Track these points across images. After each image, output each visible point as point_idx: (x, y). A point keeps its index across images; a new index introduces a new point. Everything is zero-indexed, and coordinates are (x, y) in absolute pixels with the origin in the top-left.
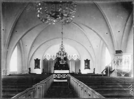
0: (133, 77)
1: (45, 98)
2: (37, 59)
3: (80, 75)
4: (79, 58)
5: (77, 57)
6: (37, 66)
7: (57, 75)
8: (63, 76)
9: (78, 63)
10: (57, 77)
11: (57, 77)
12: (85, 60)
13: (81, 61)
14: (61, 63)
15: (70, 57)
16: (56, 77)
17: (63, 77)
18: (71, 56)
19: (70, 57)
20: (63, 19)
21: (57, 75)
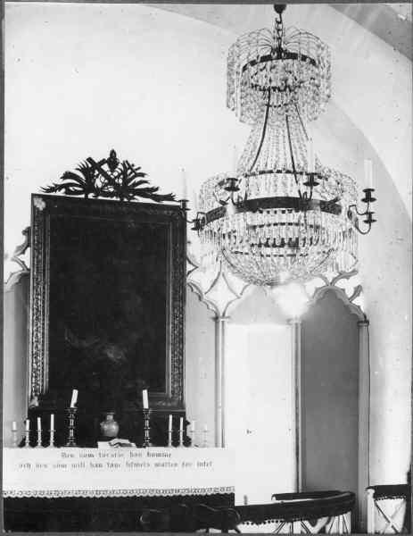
4: (347, 286)
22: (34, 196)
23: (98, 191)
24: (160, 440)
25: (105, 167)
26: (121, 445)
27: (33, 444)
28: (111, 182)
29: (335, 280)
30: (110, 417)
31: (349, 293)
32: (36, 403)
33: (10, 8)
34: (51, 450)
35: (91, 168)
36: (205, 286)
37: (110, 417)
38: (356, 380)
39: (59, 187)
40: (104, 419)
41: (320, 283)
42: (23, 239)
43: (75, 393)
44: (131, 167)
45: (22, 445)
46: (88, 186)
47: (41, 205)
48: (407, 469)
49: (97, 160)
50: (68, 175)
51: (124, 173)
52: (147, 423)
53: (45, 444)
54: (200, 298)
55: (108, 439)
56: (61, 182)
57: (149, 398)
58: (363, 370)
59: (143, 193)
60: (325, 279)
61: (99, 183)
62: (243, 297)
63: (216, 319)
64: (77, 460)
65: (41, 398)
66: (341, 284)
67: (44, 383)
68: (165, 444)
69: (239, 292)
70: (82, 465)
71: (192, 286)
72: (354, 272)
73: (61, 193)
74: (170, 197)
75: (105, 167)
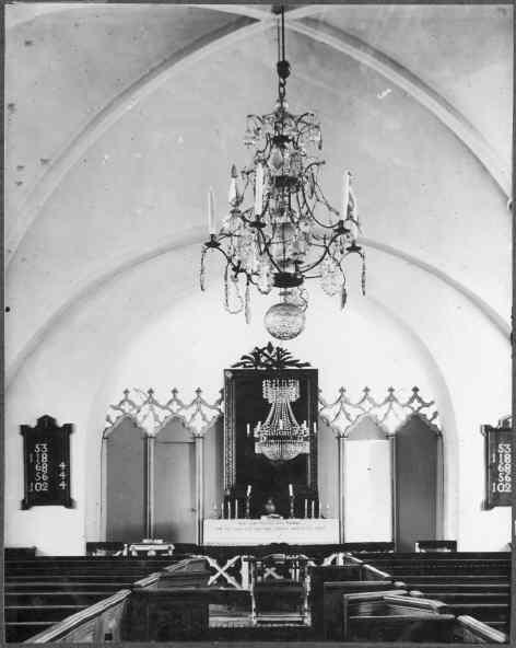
0: (493, 7)
1: (416, 645)
2: (47, 423)
3: (274, 584)
4: (428, 412)
5: (416, 404)
6: (50, 489)
7: (230, 563)
8: (235, 571)
9: (417, 451)
10: (231, 580)
11: (231, 580)
12: (488, 429)
13: (447, 437)
14: (268, 451)
15: (342, 399)
16: (221, 580)
17: (239, 579)
18: (354, 395)
19: (342, 399)
20: (282, 136)
21: (230, 563)
22: (225, 370)
23: (263, 365)
24: (300, 515)
25: (266, 351)
26: (274, 517)
27: (226, 517)
28: (270, 359)
29: (419, 408)
30: (270, 502)
31: (429, 417)
32: (228, 493)
33: (509, 7)
34: (237, 521)
35: (258, 353)
36: (331, 418)
37: (270, 502)
38: (434, 475)
39: (238, 365)
40: (267, 503)
41: (410, 412)
42: (220, 396)
43: (250, 487)
44: (281, 350)
45: (220, 518)
46: (257, 362)
47: (230, 375)
48: (511, 353)
49: (260, 348)
50: (244, 357)
51: (277, 354)
52: (292, 505)
53: (233, 517)
54: (328, 425)
55: (266, 514)
56: (240, 361)
57: (294, 490)
58: (439, 480)
59: (292, 363)
60: (412, 408)
61: (263, 359)
62: (356, 424)
63: (339, 438)
64: (247, 526)
65: (232, 490)
66: (422, 411)
67: (233, 481)
68: (302, 517)
69: (354, 419)
70: (250, 529)
71: (322, 418)
72: (432, 403)
73: (240, 368)
74: (307, 364)
75: (266, 351)
